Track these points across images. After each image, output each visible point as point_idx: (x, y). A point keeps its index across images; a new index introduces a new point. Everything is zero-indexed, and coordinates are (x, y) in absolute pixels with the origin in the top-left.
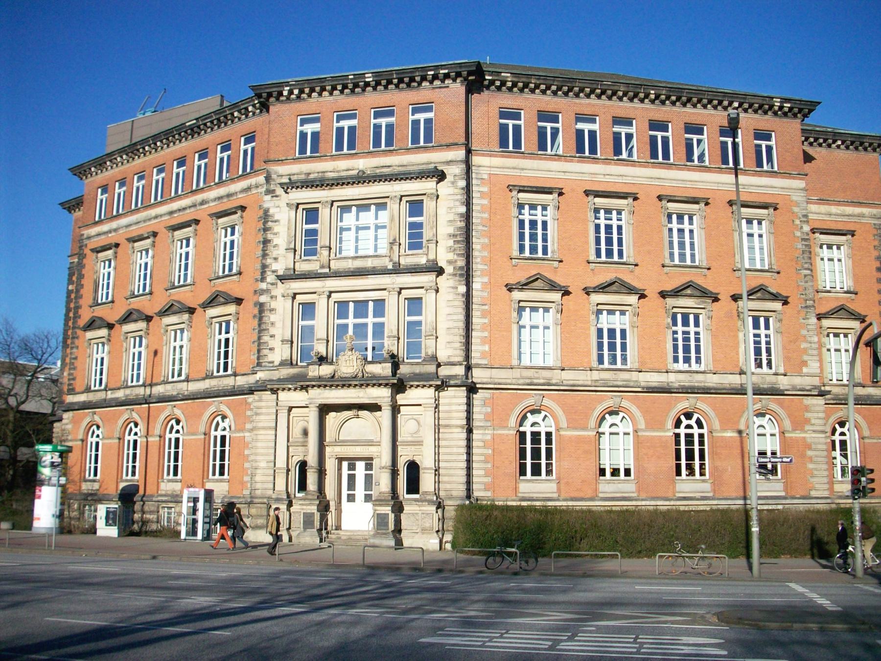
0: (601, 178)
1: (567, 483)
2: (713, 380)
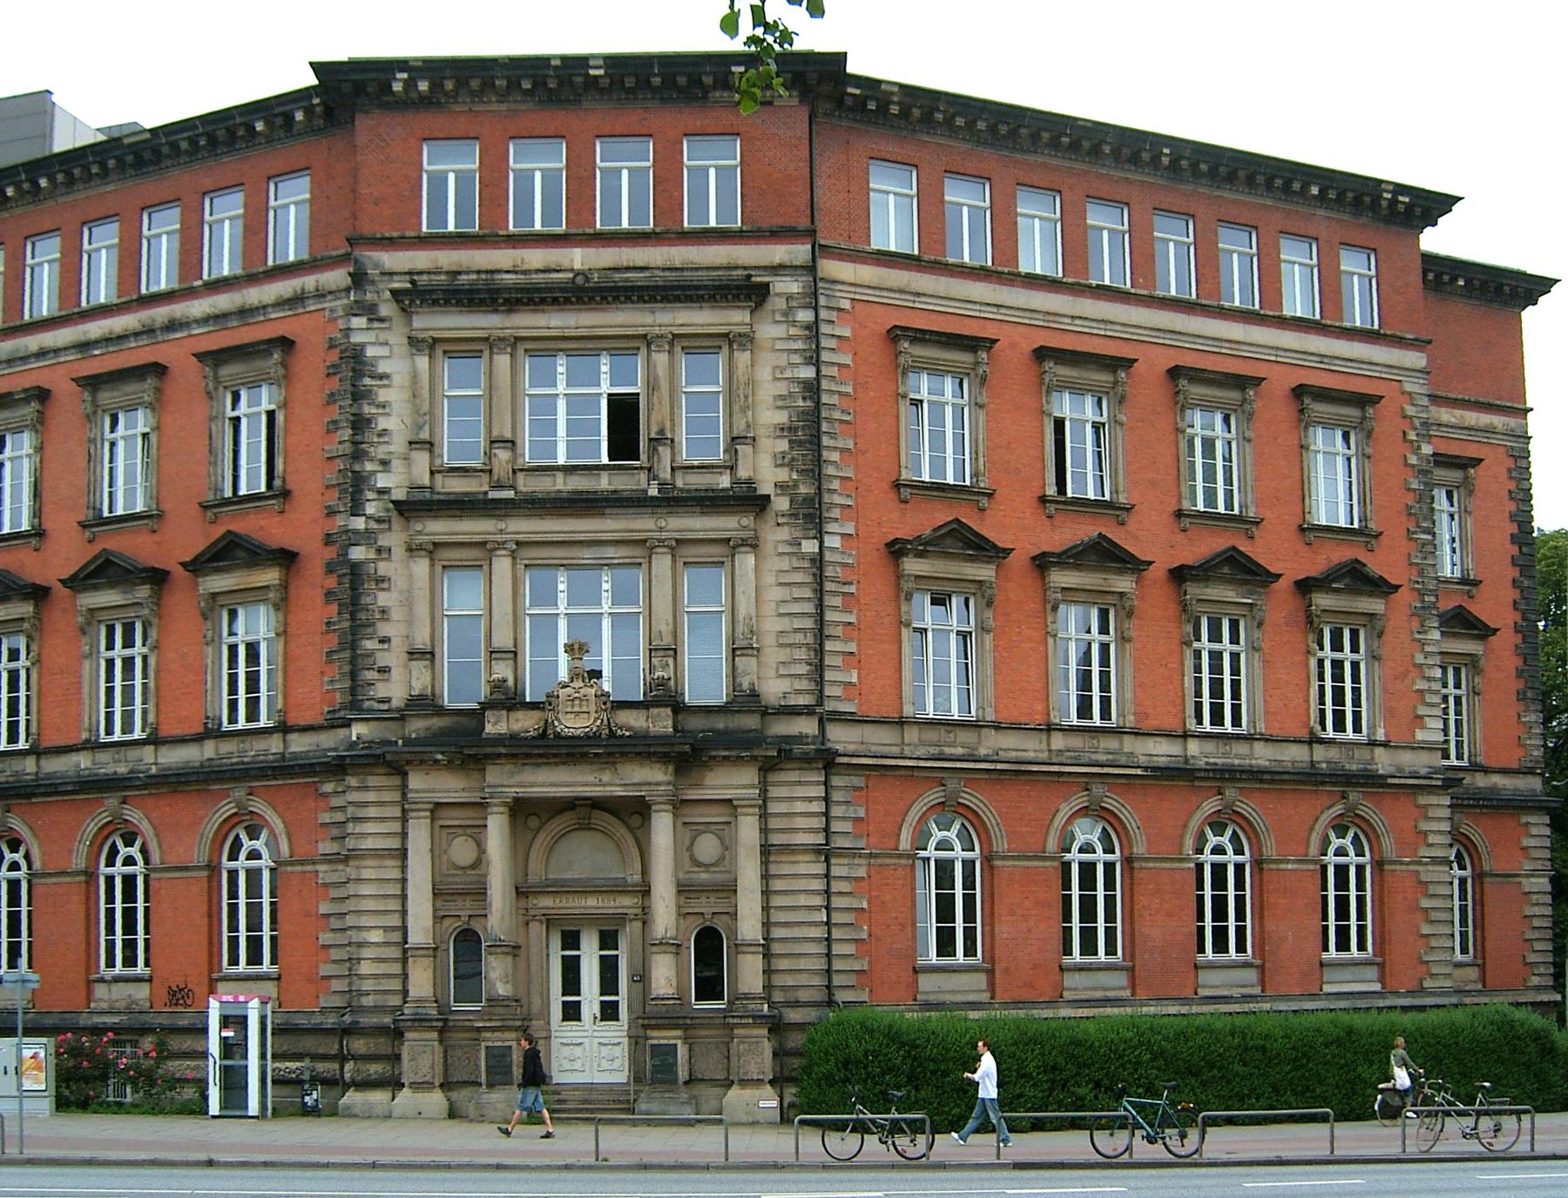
2: (1262, 755)
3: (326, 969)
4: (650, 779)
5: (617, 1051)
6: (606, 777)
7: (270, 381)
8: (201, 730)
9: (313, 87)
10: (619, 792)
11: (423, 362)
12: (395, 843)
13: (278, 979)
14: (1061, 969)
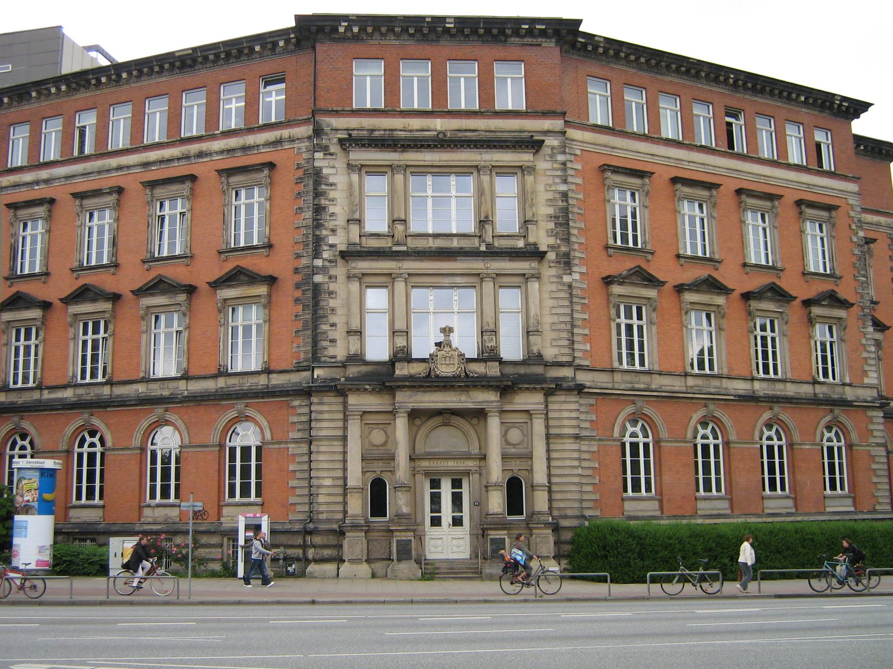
0: (685, 165)
1: (669, 500)
2: (791, 390)
3: (292, 500)
4: (488, 399)
5: (462, 542)
6: (463, 398)
7: (260, 185)
8: (216, 372)
9: (292, 28)
10: (471, 406)
11: (355, 177)
12: (340, 433)
13: (262, 505)
14: (696, 499)
